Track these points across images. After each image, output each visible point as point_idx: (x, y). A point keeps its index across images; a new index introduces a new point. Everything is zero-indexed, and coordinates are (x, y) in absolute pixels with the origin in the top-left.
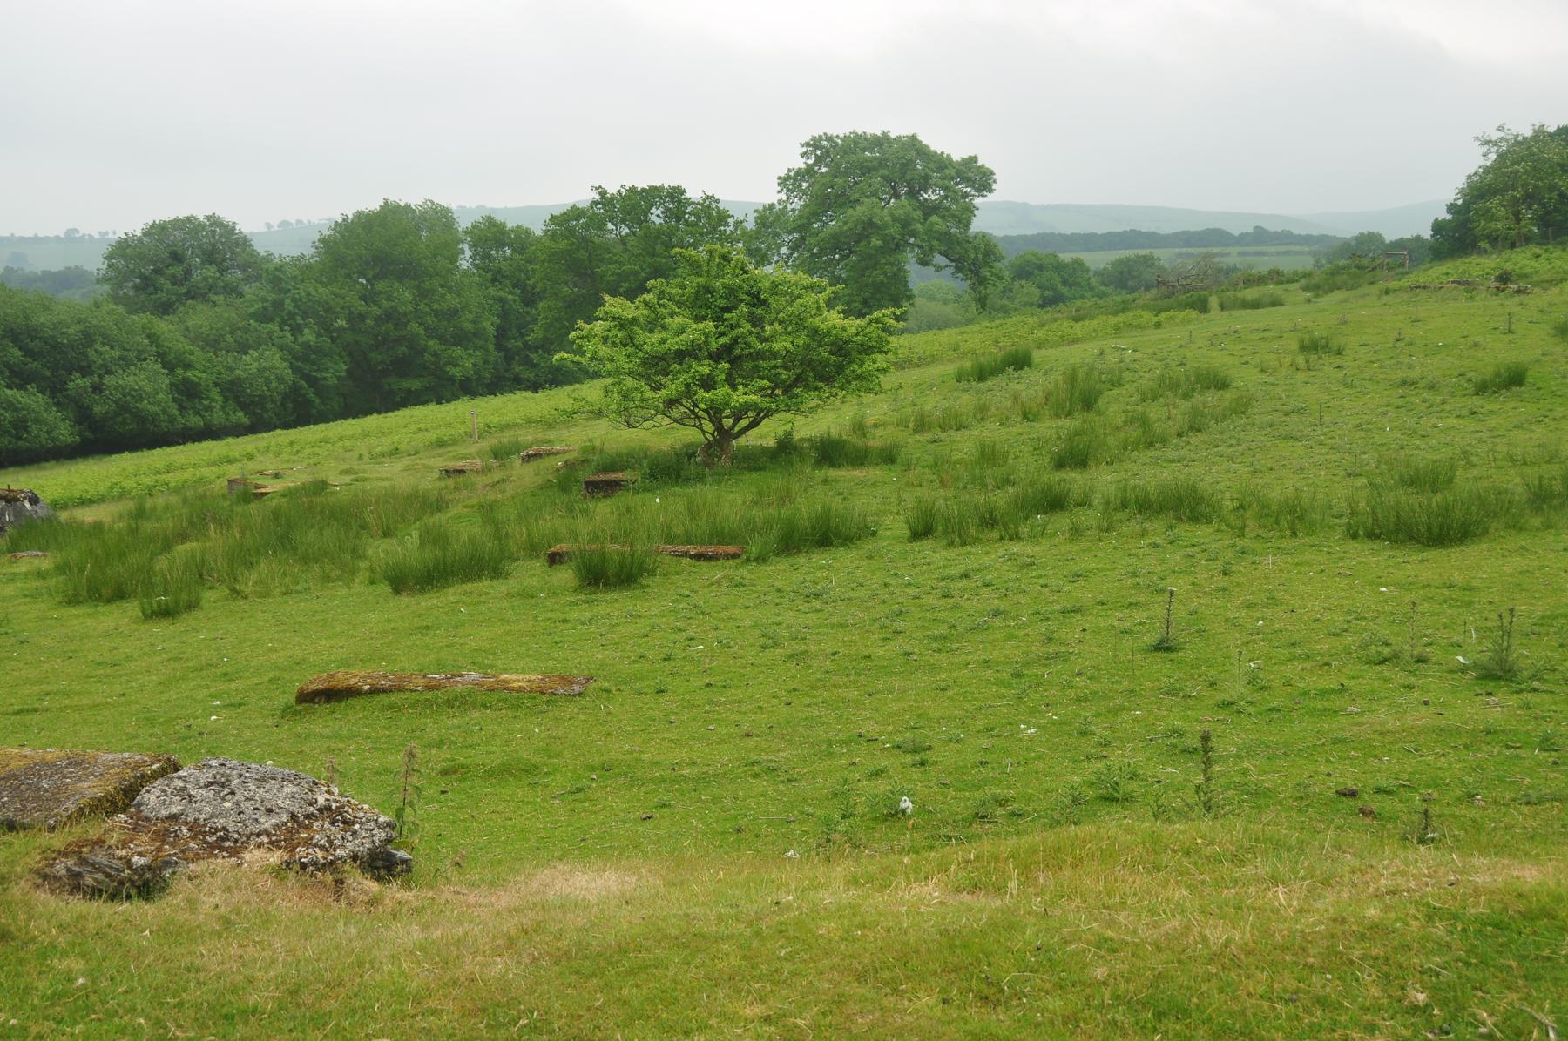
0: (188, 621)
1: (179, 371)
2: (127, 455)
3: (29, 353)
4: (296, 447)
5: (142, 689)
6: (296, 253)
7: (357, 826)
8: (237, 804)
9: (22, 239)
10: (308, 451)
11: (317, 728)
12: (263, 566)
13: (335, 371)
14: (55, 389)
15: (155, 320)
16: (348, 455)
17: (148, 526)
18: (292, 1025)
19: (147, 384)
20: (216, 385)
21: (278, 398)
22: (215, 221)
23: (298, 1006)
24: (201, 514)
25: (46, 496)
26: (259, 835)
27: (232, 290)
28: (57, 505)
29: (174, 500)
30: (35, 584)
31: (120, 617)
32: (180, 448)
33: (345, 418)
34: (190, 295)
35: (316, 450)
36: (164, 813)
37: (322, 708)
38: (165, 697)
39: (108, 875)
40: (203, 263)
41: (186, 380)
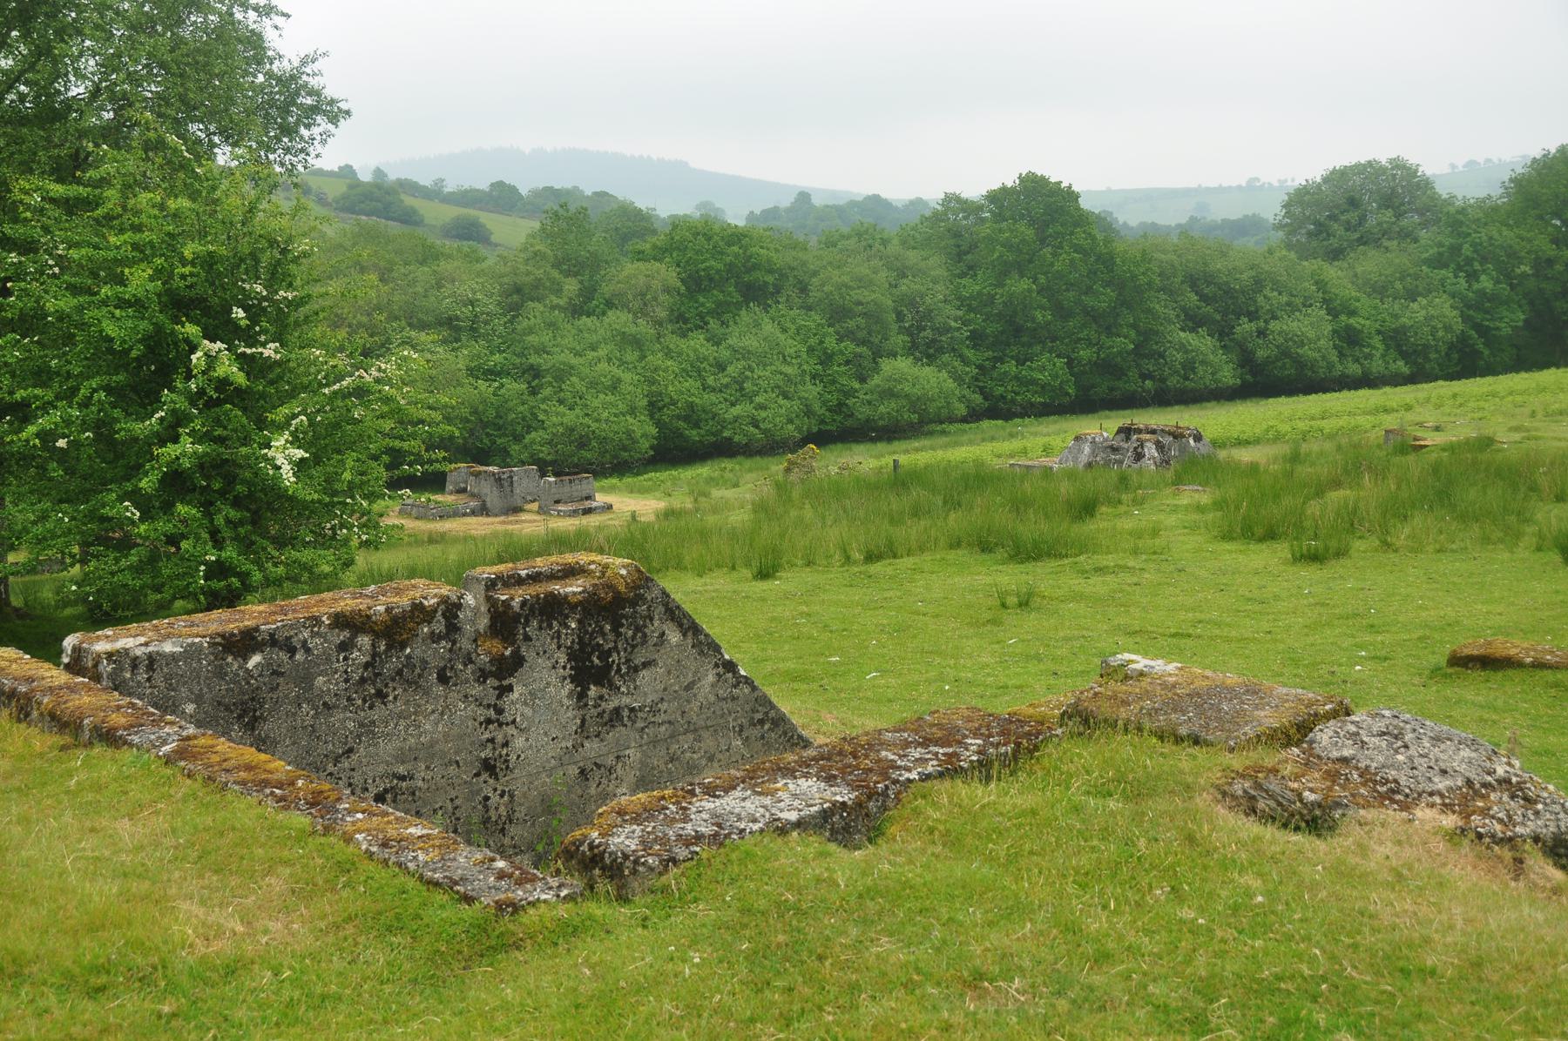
0: (1335, 568)
1: (1343, 318)
2: (1283, 399)
3: (1204, 298)
4: (1460, 400)
5: (1288, 628)
6: (1482, 194)
7: (1540, 806)
8: (1411, 758)
9: (1208, 189)
10: (1472, 404)
11: (1469, 695)
12: (1418, 520)
13: (1510, 320)
14: (1223, 333)
15: (1326, 266)
16: (1518, 411)
17: (1303, 471)
18: (1474, 998)
19: (1310, 331)
20: (1379, 332)
21: (1443, 348)
22: (1398, 164)
23: (1480, 980)
24: (1356, 463)
25: (1208, 435)
26: (1431, 794)
27: (1407, 235)
28: (1215, 444)
29: (1328, 446)
30: (1195, 517)
31: (1268, 558)
32: (1336, 395)
33: (1517, 371)
34: (1362, 241)
35: (1482, 404)
36: (1335, 754)
37: (1478, 675)
38: (1310, 640)
39: (1280, 804)
40: (1379, 208)
41: (1348, 328)
